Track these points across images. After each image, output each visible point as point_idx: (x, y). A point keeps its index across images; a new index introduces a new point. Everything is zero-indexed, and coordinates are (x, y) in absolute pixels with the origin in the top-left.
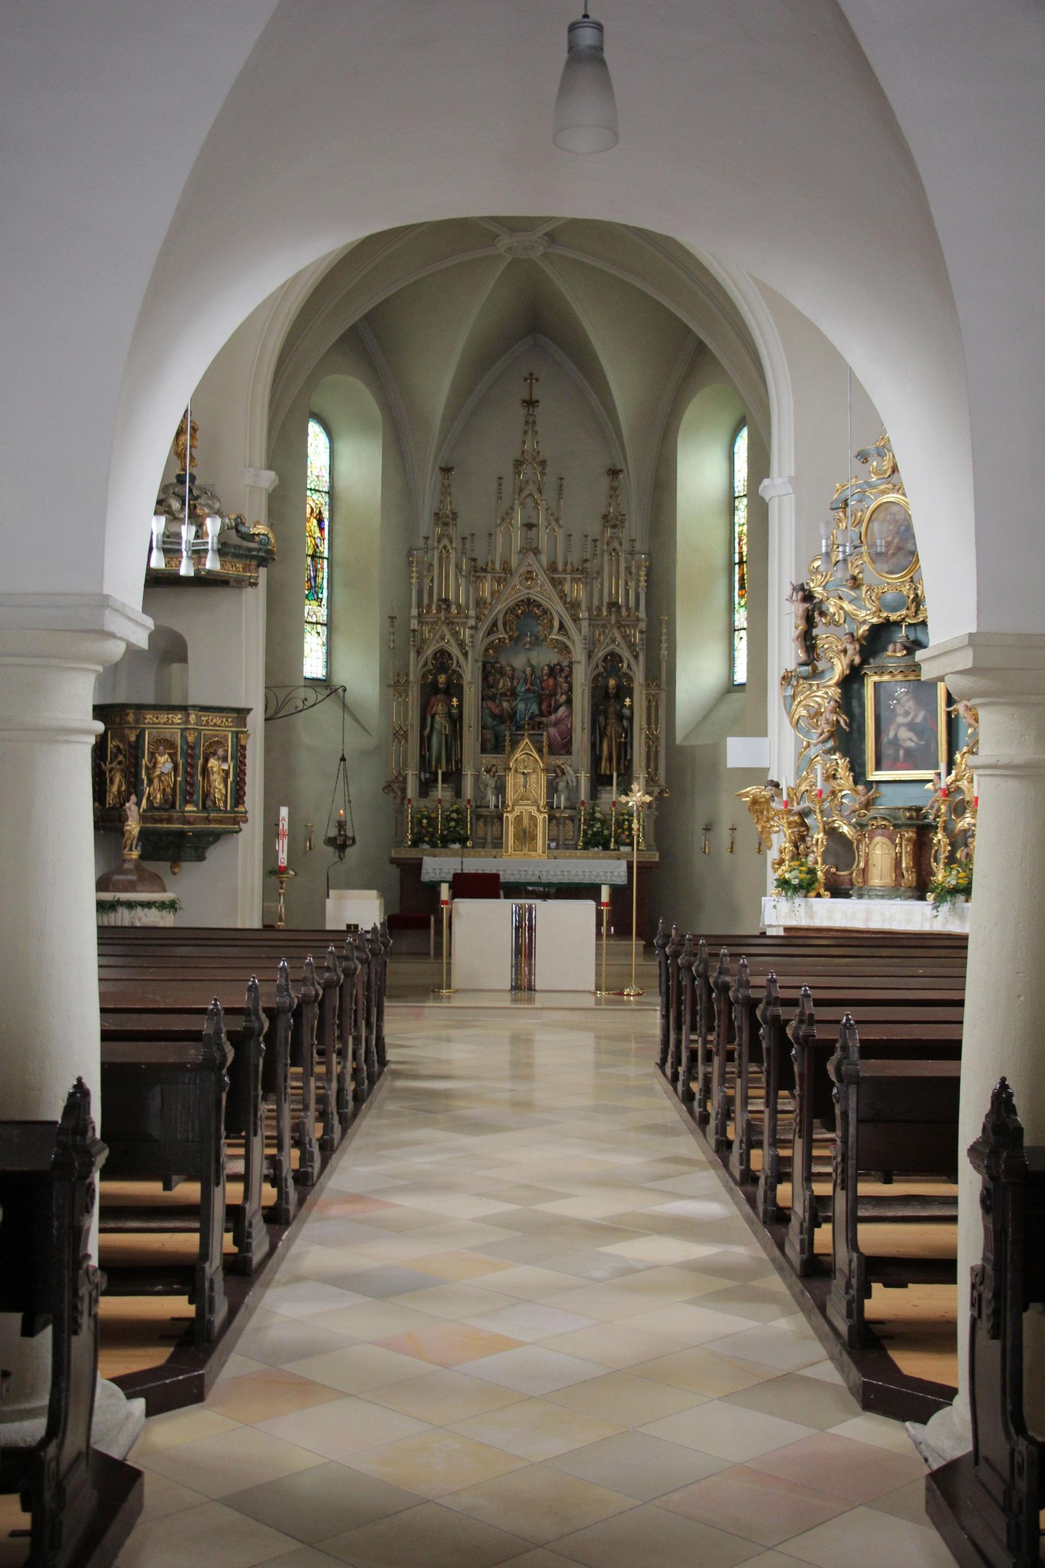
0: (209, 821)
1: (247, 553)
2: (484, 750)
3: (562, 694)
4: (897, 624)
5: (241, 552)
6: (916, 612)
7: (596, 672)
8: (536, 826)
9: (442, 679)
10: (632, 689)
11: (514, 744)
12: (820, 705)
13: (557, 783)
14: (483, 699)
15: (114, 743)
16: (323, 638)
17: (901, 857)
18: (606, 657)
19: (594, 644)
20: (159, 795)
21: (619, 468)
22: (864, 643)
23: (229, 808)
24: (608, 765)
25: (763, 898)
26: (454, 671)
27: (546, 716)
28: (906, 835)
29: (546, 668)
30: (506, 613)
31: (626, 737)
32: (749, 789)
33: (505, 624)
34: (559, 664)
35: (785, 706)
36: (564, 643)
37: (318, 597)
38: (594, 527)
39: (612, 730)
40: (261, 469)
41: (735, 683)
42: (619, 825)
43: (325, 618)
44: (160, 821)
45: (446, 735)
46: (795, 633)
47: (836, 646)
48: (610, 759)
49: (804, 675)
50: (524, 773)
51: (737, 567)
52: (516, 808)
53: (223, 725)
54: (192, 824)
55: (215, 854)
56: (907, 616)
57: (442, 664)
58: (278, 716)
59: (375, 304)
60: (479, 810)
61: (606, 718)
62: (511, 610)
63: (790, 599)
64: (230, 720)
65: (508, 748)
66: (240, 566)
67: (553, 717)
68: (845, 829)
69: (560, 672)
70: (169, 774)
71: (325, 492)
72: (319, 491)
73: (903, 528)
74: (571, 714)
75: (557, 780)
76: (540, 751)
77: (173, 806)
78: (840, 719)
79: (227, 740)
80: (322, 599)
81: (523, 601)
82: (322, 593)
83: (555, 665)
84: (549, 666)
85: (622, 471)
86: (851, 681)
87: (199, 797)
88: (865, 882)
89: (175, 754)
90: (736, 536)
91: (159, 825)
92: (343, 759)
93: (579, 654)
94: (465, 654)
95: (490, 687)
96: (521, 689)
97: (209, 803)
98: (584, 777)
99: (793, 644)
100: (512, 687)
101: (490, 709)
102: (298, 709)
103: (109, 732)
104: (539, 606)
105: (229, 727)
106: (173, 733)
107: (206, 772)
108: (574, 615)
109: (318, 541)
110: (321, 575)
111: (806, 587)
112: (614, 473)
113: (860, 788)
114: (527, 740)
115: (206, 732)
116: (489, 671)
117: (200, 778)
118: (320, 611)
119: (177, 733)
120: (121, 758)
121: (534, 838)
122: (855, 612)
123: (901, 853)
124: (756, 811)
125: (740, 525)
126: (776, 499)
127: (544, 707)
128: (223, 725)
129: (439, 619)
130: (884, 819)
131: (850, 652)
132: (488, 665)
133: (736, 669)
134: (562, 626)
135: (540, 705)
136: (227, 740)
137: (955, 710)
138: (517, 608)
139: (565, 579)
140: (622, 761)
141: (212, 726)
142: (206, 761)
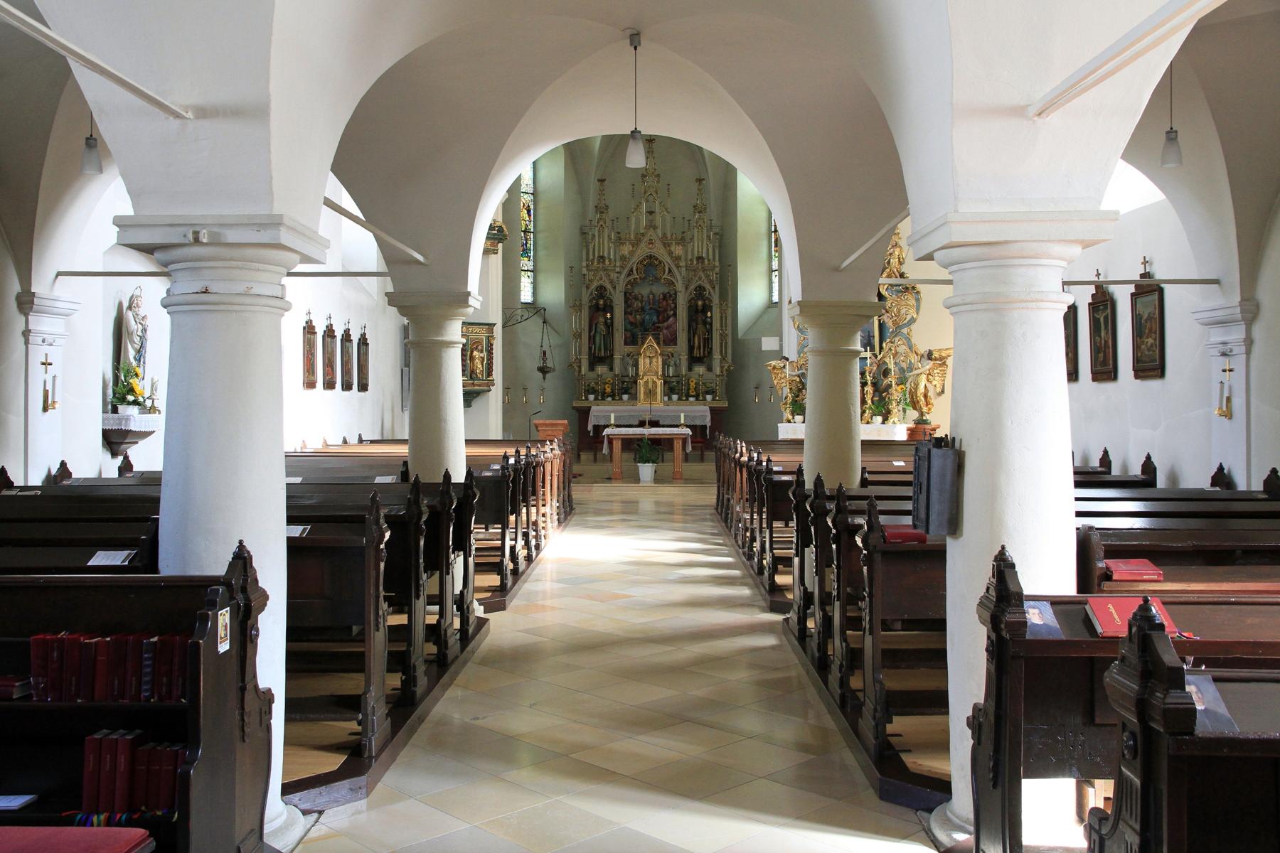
2: (626, 344)
8: (656, 387)
9: (601, 302)
10: (712, 306)
14: (625, 313)
19: (689, 281)
25: (779, 425)
31: (708, 334)
33: (637, 270)
34: (669, 293)
36: (671, 281)
57: (601, 294)
65: (640, 343)
69: (670, 297)
74: (675, 323)
75: (670, 360)
76: (658, 344)
84: (663, 294)
93: (680, 286)
94: (615, 288)
98: (684, 357)
104: (657, 259)
107: (472, 358)
112: (700, 181)
116: (628, 297)
117: (469, 362)
124: (775, 373)
127: (660, 318)
134: (670, 271)
135: (658, 317)
139: (672, 243)
142: (472, 352)
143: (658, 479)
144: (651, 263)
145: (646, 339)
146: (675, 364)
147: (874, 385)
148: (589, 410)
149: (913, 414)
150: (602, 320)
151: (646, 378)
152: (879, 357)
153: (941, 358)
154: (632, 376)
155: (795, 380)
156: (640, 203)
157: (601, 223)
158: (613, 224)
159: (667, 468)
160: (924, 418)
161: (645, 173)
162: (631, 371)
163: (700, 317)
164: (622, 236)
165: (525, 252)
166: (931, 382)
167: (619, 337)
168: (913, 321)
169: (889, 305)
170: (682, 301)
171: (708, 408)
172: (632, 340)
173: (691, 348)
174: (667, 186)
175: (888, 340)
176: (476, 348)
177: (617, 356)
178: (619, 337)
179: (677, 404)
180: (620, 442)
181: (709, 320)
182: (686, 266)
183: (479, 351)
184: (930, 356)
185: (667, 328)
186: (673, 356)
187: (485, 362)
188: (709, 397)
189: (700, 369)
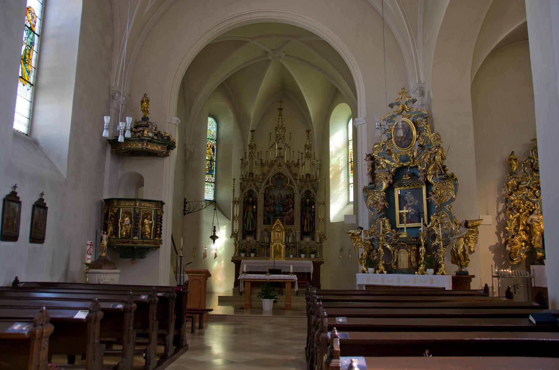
0: (144, 243)
1: (162, 142)
2: (264, 223)
3: (291, 204)
4: (406, 167)
5: (160, 142)
6: (413, 162)
8: (281, 249)
9: (251, 199)
10: (315, 203)
11: (274, 222)
12: (378, 199)
13: (289, 234)
14: (264, 206)
15: (111, 213)
16: (213, 188)
17: (411, 257)
18: (306, 192)
19: (301, 188)
20: (124, 233)
21: (309, 130)
22: (394, 174)
23: (152, 238)
24: (306, 228)
25: (357, 274)
26: (254, 197)
27: (286, 212)
28: (413, 248)
29: (286, 196)
30: (272, 177)
31: (312, 219)
32: (351, 231)
33: (272, 181)
34: (290, 194)
35: (365, 200)
36: (291, 187)
37: (212, 174)
38: (302, 149)
39: (308, 215)
40: (173, 117)
41: (350, 201)
43: (214, 181)
44: (124, 243)
45: (252, 219)
46: (367, 172)
47: (383, 177)
49: (371, 188)
50: (278, 231)
51: (350, 163)
52: (274, 243)
53: (150, 207)
54: (137, 244)
55: (150, 257)
56: (410, 164)
57: (251, 194)
58: (194, 211)
59: (227, 77)
60: (262, 243)
61: (306, 213)
62: (274, 177)
63: (366, 160)
64: (153, 205)
65: (272, 223)
66: (160, 147)
67: (288, 212)
68: (388, 246)
69: (291, 197)
70: (128, 225)
71: (215, 140)
72: (213, 140)
73: (407, 130)
74: (293, 212)
75: (289, 233)
76: (283, 224)
77: (130, 237)
78: (385, 204)
79: (152, 212)
80: (213, 174)
81: (278, 173)
82: (213, 173)
83: (288, 195)
84: (286, 195)
85: (310, 130)
86: (390, 189)
87: (140, 233)
88: (397, 267)
89: (131, 217)
90: (350, 153)
91: (124, 244)
93: (296, 191)
94: (258, 191)
95: (266, 202)
96: (277, 203)
97: (144, 236)
98: (298, 231)
99: (367, 176)
101: (266, 209)
102: (200, 209)
103: (110, 210)
104: (283, 175)
105: (153, 207)
106: (131, 209)
107: (143, 224)
108: (295, 178)
109: (212, 156)
110: (213, 167)
111: (372, 155)
112: (308, 131)
113: (394, 230)
114: (278, 220)
115: (143, 209)
116: (266, 196)
117: (140, 227)
118: (212, 179)
119: (132, 209)
120: (112, 219)
121: (281, 253)
122: (387, 223)
123: (411, 255)
124: (354, 239)
125: (351, 150)
126: (359, 126)
127: (285, 209)
128: (150, 207)
129: (250, 179)
130: (404, 242)
131: (389, 178)
132: (266, 195)
133: (350, 197)
134: (291, 182)
135: (283, 208)
136: (152, 212)
137: (430, 199)
138: (276, 176)
139: (292, 166)
140: (311, 227)
141: (146, 207)
142: (143, 220)
143: (276, 311)
144: (279, 177)
145: (276, 221)
146: (293, 236)
147: (426, 246)
148: (241, 262)
149: (456, 268)
150: (250, 209)
151: (275, 244)
152: (428, 226)
153: (474, 227)
154: (267, 242)
155: (368, 243)
156: (274, 143)
157: (252, 154)
158: (258, 155)
159: (282, 301)
160: (463, 270)
161: (277, 127)
162: (266, 240)
163: (308, 209)
164: (264, 162)
165: (210, 172)
166: (467, 244)
167: (260, 220)
168: (452, 200)
169: (435, 189)
170: (298, 199)
171: (311, 262)
172: (268, 222)
173: (302, 227)
174: (290, 134)
175: (435, 214)
176: (146, 218)
177: (259, 230)
178: (260, 220)
179: (293, 260)
180: (250, 284)
181: (313, 210)
182: (300, 179)
183: (148, 220)
184: (466, 224)
185: (289, 215)
186: (291, 231)
187: (153, 227)
188: (313, 256)
189: (307, 239)
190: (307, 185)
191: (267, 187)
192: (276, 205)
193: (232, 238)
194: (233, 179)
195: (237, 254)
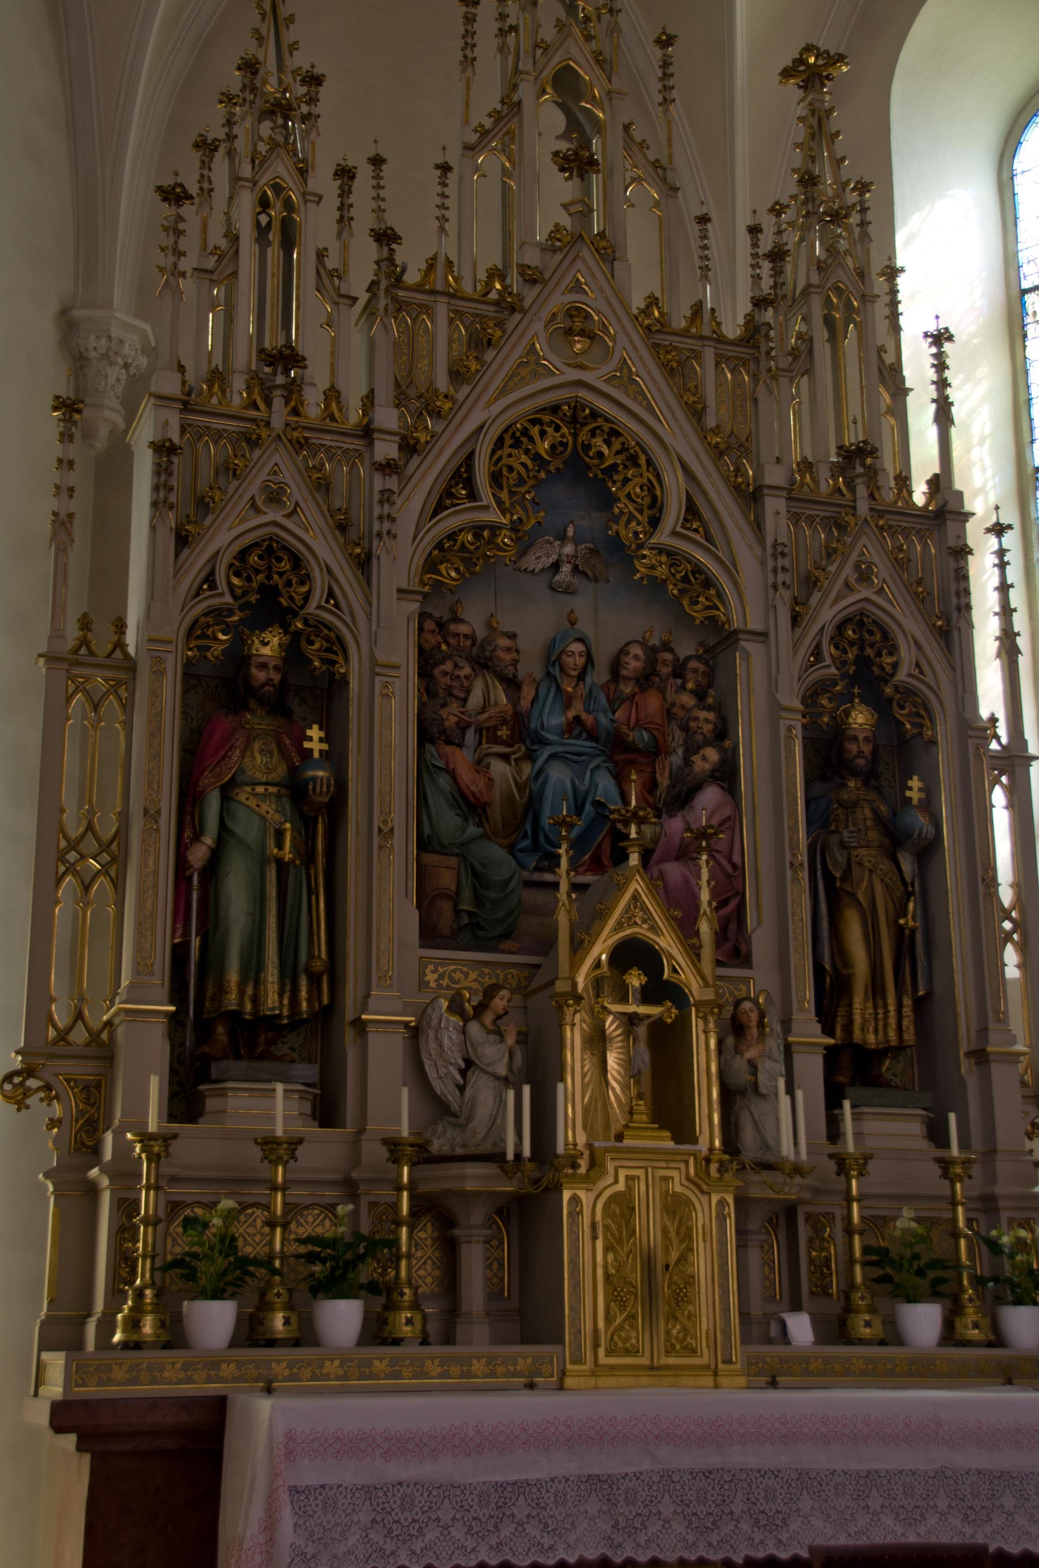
7: (817, 675)
26: (317, 626)
29: (636, 650)
30: (500, 442)
42: (311, 1258)
48: (876, 989)
57: (270, 593)
81: (555, 409)
92: (376, 142)
94: (364, 564)
100: (516, 714)
101: (453, 774)
114: (637, 885)
139: (697, 356)
174: (658, 52)
190: (854, 558)
191: (452, 536)
192: (544, 743)
193: (21, 1105)
194: (438, 167)
195: (138, 1309)
